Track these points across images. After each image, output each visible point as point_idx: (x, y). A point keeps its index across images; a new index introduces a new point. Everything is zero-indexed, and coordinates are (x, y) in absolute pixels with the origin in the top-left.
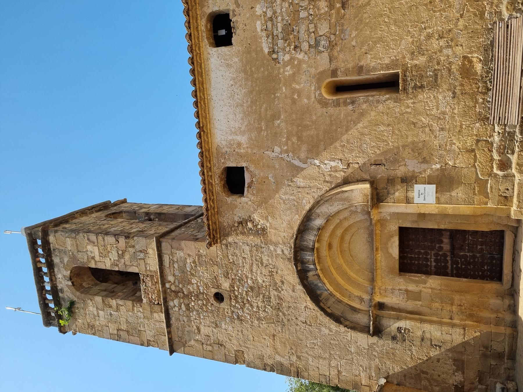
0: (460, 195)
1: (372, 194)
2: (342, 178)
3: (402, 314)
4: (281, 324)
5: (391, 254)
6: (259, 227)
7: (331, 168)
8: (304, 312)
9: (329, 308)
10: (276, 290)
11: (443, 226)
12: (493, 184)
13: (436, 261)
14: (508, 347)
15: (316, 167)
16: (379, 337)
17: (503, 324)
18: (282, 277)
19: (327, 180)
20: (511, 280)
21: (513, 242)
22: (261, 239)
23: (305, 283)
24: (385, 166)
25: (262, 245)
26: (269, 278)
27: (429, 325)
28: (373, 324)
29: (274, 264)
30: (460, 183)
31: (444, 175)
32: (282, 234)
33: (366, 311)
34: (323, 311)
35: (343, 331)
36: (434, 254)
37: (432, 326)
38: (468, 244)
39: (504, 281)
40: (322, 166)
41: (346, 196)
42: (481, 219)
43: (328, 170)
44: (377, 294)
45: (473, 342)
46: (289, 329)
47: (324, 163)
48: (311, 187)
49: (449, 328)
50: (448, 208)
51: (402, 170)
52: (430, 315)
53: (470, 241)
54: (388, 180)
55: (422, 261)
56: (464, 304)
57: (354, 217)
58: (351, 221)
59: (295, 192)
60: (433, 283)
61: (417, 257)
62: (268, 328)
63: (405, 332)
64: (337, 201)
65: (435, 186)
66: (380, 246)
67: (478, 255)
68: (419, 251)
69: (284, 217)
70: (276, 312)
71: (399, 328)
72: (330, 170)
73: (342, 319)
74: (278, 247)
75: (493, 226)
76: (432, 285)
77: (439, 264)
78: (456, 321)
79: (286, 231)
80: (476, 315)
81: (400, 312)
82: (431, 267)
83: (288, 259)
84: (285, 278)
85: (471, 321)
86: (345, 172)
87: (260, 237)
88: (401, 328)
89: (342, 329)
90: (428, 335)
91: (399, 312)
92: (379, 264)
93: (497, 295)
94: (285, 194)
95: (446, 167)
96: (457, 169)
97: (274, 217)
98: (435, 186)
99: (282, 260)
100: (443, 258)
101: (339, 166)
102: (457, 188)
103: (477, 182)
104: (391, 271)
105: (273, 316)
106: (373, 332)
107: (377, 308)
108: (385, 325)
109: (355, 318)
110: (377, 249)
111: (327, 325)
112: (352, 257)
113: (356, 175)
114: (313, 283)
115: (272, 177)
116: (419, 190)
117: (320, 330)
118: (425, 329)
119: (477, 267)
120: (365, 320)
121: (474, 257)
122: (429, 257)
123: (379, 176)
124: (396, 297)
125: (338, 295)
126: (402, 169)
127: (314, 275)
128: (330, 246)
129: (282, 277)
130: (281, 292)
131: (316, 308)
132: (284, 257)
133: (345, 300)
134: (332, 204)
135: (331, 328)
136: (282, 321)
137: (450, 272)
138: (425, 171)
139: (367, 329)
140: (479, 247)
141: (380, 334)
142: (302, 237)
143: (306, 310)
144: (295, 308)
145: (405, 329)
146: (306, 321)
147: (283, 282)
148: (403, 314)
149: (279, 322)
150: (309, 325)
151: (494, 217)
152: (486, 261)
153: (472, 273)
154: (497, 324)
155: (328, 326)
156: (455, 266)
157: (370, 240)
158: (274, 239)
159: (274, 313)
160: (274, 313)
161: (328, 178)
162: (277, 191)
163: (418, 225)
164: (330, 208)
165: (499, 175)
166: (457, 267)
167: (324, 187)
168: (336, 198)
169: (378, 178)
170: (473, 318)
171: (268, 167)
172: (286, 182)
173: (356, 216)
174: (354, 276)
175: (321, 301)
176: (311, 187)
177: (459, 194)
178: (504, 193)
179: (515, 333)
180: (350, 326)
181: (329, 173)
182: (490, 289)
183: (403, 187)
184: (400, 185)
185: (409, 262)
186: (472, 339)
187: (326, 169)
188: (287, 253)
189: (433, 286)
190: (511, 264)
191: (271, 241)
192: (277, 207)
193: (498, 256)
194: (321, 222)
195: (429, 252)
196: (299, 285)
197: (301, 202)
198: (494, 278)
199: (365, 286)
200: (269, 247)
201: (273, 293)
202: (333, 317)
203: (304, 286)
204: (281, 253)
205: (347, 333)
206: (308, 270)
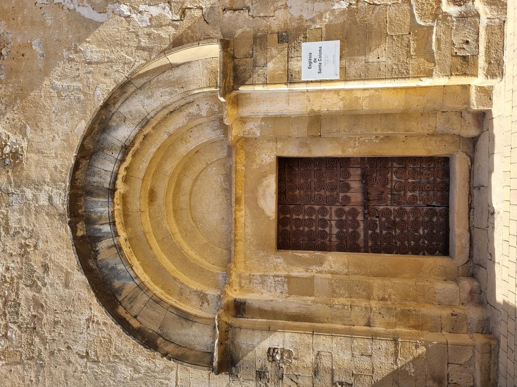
0: (384, 59)
1: (224, 65)
2: (171, 39)
3: (277, 321)
4: (37, 364)
5: (263, 210)
6: (7, 150)
7: (150, 19)
8: (84, 331)
9: (135, 317)
10: (31, 286)
11: (350, 150)
12: (442, 34)
13: (341, 224)
14: (482, 374)
15: (123, 19)
16: (231, 374)
17: (465, 330)
18: (45, 256)
19: (143, 44)
20: (468, 246)
21: (468, 172)
22: (8, 176)
23: (91, 264)
24: (249, 11)
25: (10, 189)
26: (19, 260)
27: (329, 339)
28: (220, 344)
29: (31, 228)
30: (383, 36)
31: (355, 23)
32: (51, 163)
33: (209, 319)
34: (120, 324)
35: (161, 367)
36: (336, 212)
37: (335, 340)
38: (391, 190)
39: (456, 249)
40: (134, 16)
41: (177, 76)
42: (415, 124)
43: (145, 25)
44: (235, 288)
45: (413, 370)
46: (51, 373)
47: (137, 10)
48: (112, 62)
49: (366, 341)
51: (280, 16)
52: (330, 320)
53: (393, 184)
54: (255, 38)
55: (316, 227)
56: (390, 296)
57: (198, 135)
58: (192, 144)
59: (81, 72)
60: (335, 262)
61: (308, 219)
62: (8, 375)
63: (282, 358)
64: (160, 87)
65: (339, 42)
66: (243, 197)
67: (408, 209)
69: (58, 127)
70: (29, 337)
71: (272, 350)
72: (149, 24)
73: (160, 340)
74: (41, 190)
75: (434, 145)
76: (333, 265)
77: (345, 230)
78: (379, 328)
79: (59, 156)
80: (414, 312)
81: (275, 318)
82: (331, 238)
83: (60, 215)
84: (51, 259)
85: (405, 327)
86: (176, 27)
87: (8, 172)
88: (274, 349)
89: (161, 362)
90: (326, 362)
91: (274, 319)
92: (240, 231)
93: (445, 278)
94: (63, 76)
95: (359, 6)
96: (378, 8)
97: (38, 127)
98: (339, 42)
99: (47, 218)
100: (350, 218)
101: (165, 16)
102: (378, 46)
103: (414, 32)
104: (261, 245)
105: (21, 346)
106: (220, 363)
107: (231, 313)
108: (244, 346)
109: (185, 335)
110: (238, 201)
111: (130, 357)
112: (194, 221)
113: (197, 32)
114: (107, 264)
115: (39, 44)
116: (310, 54)
117: (115, 371)
118: (321, 349)
119: (406, 231)
120: (205, 338)
121: (401, 212)
122: (327, 217)
123: (239, 32)
124: (270, 291)
125: (158, 291)
126: (280, 14)
127: (109, 248)
128: (152, 196)
129: (45, 256)
130: (41, 289)
131: (110, 321)
132: (53, 211)
133: (172, 301)
134: (150, 94)
135: (137, 365)
136: (38, 356)
137: (362, 245)
138: (321, 16)
139: (207, 359)
140: (409, 194)
141: (233, 368)
142: (90, 166)
143: (88, 327)
144: (69, 324)
145: (283, 351)
146: (87, 353)
147: (46, 268)
148: (280, 321)
149: (31, 358)
150: (94, 361)
151: (438, 120)
152: (421, 219)
153: (399, 243)
154: (454, 330)
155: (132, 360)
157: (226, 186)
158: (34, 174)
159: (23, 340)
160: (23, 340)
161: (144, 42)
162: (46, 72)
163: (310, 151)
164: (146, 102)
165: (451, 16)
166: (374, 233)
167: (138, 60)
168: (158, 82)
169: (236, 36)
170: (409, 320)
171: (33, 23)
172: (65, 54)
173: (201, 132)
174: (197, 257)
175: (121, 304)
176: (112, 62)
177: (381, 59)
178: (462, 50)
179: (493, 343)
180: (175, 353)
181: (146, 31)
182: (432, 267)
183: (281, 51)
184: (277, 48)
185: (294, 228)
186: (412, 362)
187: (142, 21)
188: (58, 203)
189: (335, 267)
190: (467, 215)
191: (28, 178)
192: (45, 106)
193: (440, 208)
194: (129, 133)
195: (328, 207)
197: (91, 93)
198: (436, 251)
199: (212, 272)
200: (23, 191)
201: (25, 293)
202: (140, 337)
203: (87, 270)
204: (46, 203)
205: (169, 373)
206: (99, 237)
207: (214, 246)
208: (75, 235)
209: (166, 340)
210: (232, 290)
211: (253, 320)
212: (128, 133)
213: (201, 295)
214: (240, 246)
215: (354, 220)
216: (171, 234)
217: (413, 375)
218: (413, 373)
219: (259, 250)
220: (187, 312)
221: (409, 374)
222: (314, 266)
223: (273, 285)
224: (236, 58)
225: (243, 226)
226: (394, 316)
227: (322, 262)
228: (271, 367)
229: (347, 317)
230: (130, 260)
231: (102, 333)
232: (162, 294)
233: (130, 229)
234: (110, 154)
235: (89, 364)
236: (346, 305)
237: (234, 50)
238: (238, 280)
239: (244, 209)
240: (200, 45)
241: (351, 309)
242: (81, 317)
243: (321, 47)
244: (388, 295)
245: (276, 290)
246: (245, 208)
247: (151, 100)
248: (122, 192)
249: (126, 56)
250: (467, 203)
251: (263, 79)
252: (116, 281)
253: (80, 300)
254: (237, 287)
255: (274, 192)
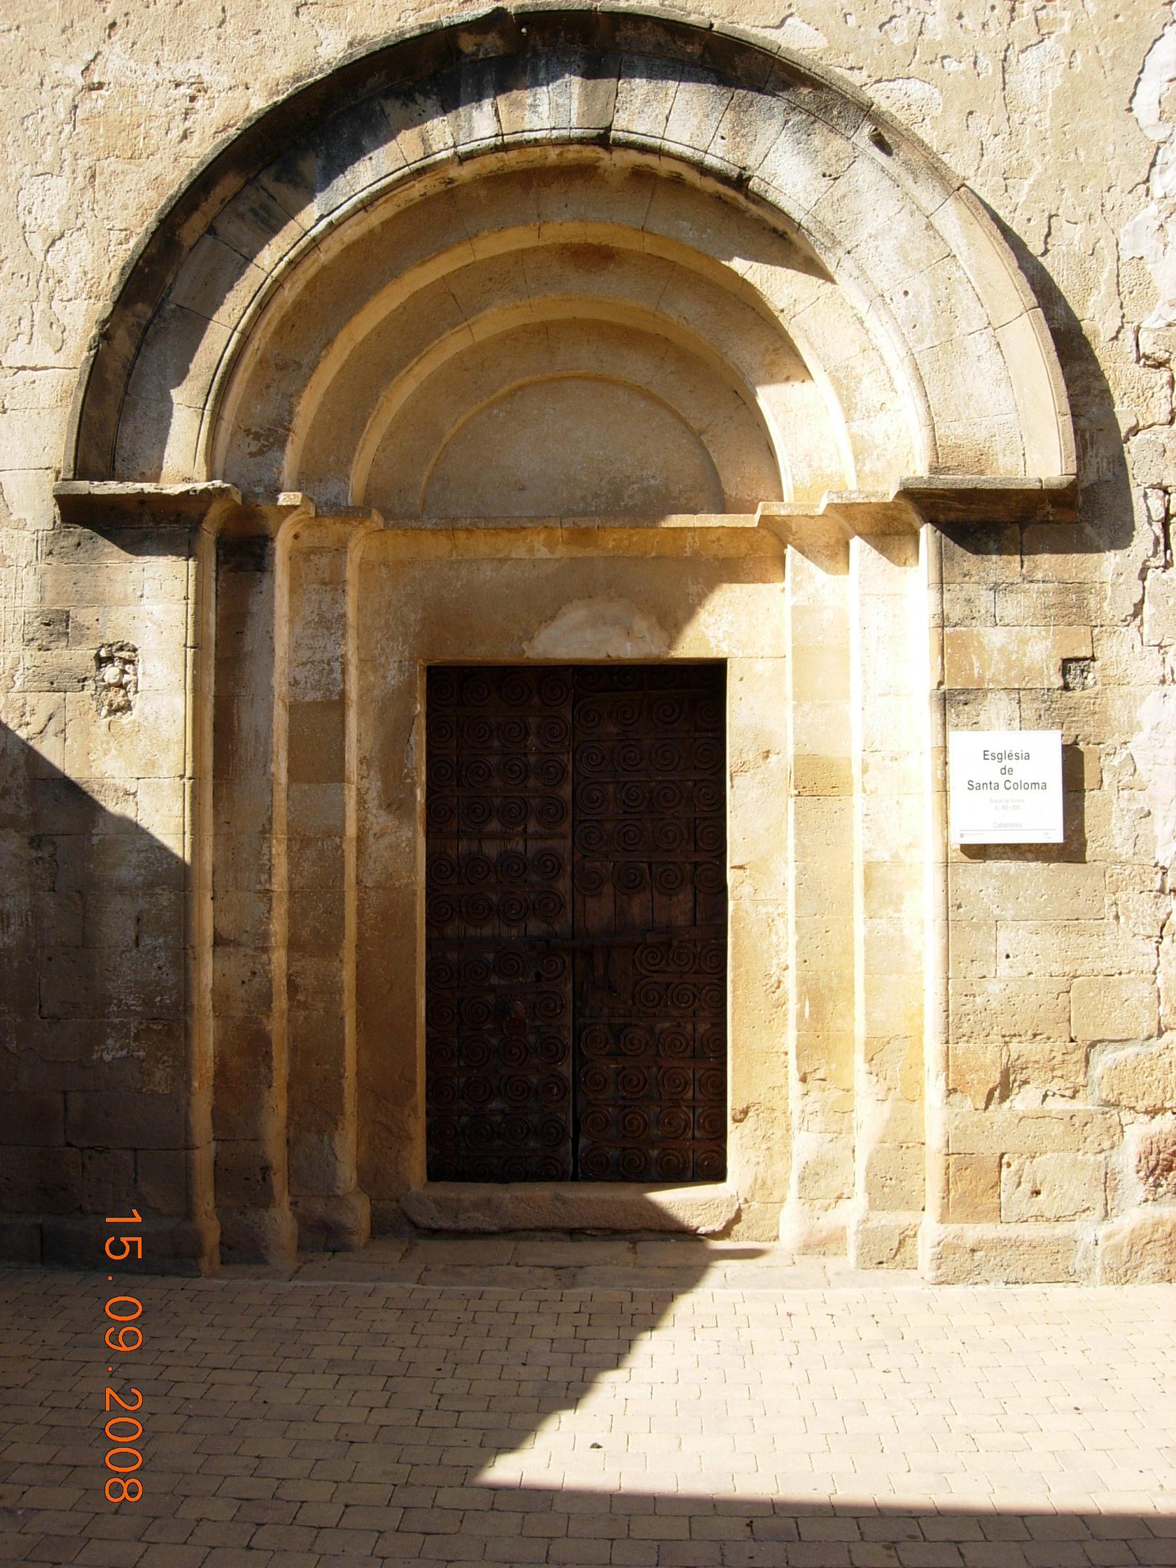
5: (553, 618)
9: (211, 230)
40: (1153, 208)
45: (107, 1057)
50: (898, 911)
60: (393, 847)
68: (564, 770)
76: (385, 841)
112: (512, 394)
116: (1028, 757)
122: (533, 827)
137: (450, 931)
156: (491, 957)
157: (631, 497)
169: (1089, 529)
175: (248, 182)
184: (1049, 657)
194: (788, 189)
196: (351, 44)
207: (433, 460)
208: (463, 31)
209: (146, 330)
210: (297, 529)
211: (213, 596)
212: (790, 186)
213: (280, 430)
214: (436, 547)
215: (528, 907)
216: (469, 322)
217: (94, 1057)
218: (101, 1057)
219: (424, 609)
220: (229, 391)
221: (96, 1048)
222: (379, 784)
223: (317, 657)
224: (1022, 529)
225: (501, 555)
226: (250, 1012)
227: (394, 807)
228: (394, 678)
229: (235, 878)
230: (385, 202)
231: (159, 127)
232: (280, 307)
233: (483, 193)
234: (721, 132)
235: (69, 92)
236: (270, 877)
237: (1048, 522)
238: (327, 543)
239: (557, 556)
240: (1061, 419)
241: (260, 892)
242: (207, 60)
243: (1045, 786)
244: (305, 1002)
245: (304, 664)
246: (557, 560)
247: (895, 259)
248: (601, 163)
249: (1031, 182)
250: (585, 1224)
251: (955, 614)
252: (320, 163)
253: (260, 54)
254: (307, 540)
255: (613, 655)
